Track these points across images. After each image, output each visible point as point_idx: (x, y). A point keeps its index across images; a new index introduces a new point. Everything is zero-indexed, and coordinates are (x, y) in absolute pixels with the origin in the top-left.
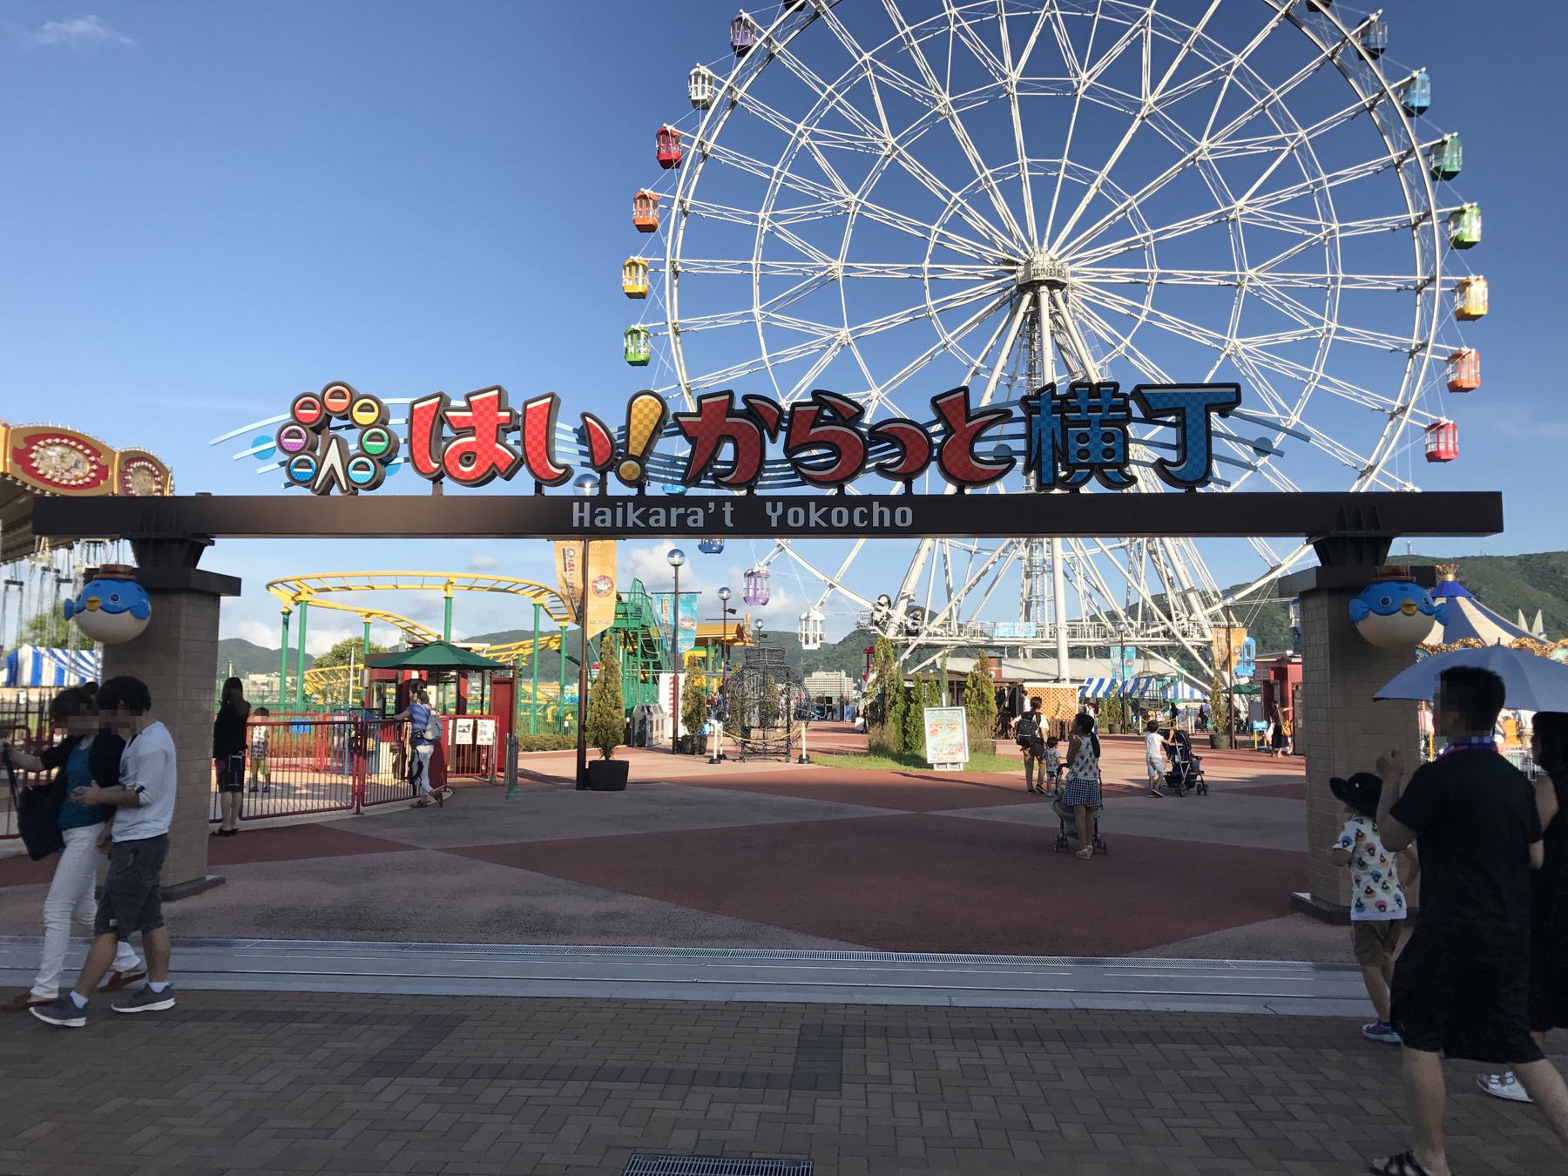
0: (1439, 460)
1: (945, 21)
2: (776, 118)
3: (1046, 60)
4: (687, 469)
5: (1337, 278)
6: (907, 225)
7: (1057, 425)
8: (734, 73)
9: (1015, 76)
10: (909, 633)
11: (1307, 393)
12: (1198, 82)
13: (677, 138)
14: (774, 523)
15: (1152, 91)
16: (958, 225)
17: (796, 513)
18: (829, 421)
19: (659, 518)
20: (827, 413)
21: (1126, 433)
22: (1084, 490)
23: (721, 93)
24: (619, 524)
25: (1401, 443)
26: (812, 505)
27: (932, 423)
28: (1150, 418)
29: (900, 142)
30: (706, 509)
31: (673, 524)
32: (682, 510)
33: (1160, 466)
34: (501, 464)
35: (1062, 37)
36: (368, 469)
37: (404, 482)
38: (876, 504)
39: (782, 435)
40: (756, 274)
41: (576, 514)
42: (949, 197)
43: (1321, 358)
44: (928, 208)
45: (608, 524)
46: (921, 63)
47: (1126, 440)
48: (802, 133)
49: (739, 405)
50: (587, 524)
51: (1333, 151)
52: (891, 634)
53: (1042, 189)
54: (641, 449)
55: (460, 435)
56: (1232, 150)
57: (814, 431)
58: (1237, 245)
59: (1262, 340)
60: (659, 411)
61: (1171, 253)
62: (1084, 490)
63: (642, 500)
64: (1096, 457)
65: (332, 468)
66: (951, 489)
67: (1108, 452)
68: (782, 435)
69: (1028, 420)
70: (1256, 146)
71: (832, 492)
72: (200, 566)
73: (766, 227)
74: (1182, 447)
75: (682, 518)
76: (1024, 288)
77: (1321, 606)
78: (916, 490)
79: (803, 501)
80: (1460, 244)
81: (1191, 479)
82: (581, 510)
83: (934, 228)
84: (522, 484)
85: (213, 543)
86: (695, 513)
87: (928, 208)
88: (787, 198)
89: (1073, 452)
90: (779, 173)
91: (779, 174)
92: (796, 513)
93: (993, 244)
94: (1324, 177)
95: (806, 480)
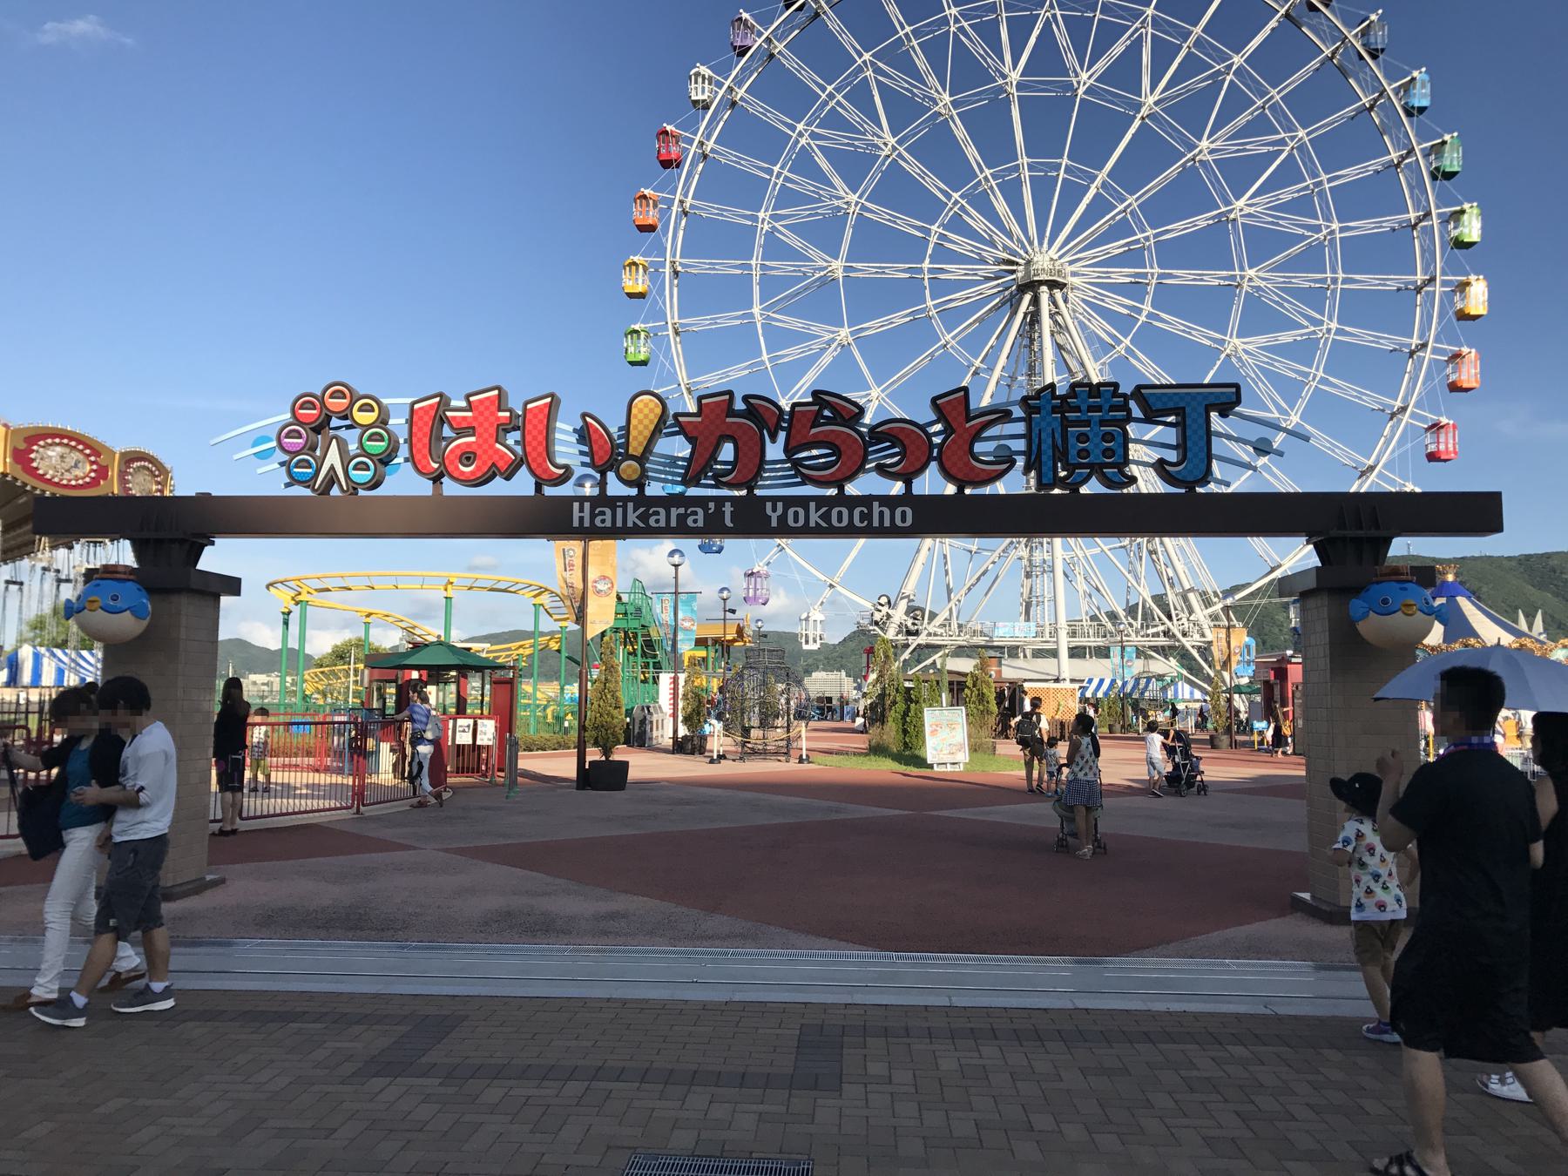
0: (1439, 460)
1: (945, 21)
2: (776, 118)
3: (1046, 60)
4: (687, 469)
5: (1337, 278)
6: (907, 225)
7: (1057, 425)
8: (734, 73)
9: (1015, 76)
10: (909, 633)
11: (1307, 393)
12: (1198, 82)
13: (677, 138)
14: (774, 523)
15: (1152, 91)
16: (958, 225)
17: (796, 513)
18: (829, 421)
19: (659, 518)
20: (827, 413)
21: (1126, 433)
22: (1084, 490)
23: (721, 93)
24: (619, 524)
25: (1401, 443)
26: (812, 505)
27: (932, 423)
28: (1150, 418)
29: (900, 142)
30: (706, 509)
31: (673, 524)
32: (682, 510)
33: (1160, 466)
34: (501, 464)
35: (1062, 37)
36: (368, 469)
37: (404, 482)
38: (876, 504)
39: (782, 435)
40: (756, 274)
41: (576, 514)
42: (949, 197)
43: (1321, 358)
44: (928, 208)
45: (608, 524)
46: (921, 63)
47: (1126, 440)
48: (802, 133)
49: (739, 405)
50: (587, 524)
51: (1333, 151)
52: (891, 634)
53: (1042, 189)
54: (641, 449)
55: (460, 435)
56: (1232, 150)
57: (814, 431)
58: (1237, 245)
59: (1262, 340)
60: (659, 411)
61: (1171, 253)
62: (1084, 490)
63: (642, 500)
64: (1096, 457)
65: (332, 468)
66: (951, 489)
67: (1108, 452)
68: (782, 435)
69: (1028, 420)
70: (1256, 146)
71: (832, 492)
72: (200, 566)
73: (766, 227)
74: (1182, 447)
75: (682, 518)
76: (1024, 288)
77: (1321, 606)
78: (916, 490)
79: (803, 501)
80: (1460, 244)
81: (1191, 479)
82: (581, 510)
83: (934, 228)
84: (522, 484)
85: (213, 543)
86: (695, 513)
87: (928, 208)
88: (787, 198)
89: (1073, 452)
90: (779, 173)
91: (779, 174)
92: (796, 513)
93: (993, 244)
94: (1324, 177)
95: (806, 480)
